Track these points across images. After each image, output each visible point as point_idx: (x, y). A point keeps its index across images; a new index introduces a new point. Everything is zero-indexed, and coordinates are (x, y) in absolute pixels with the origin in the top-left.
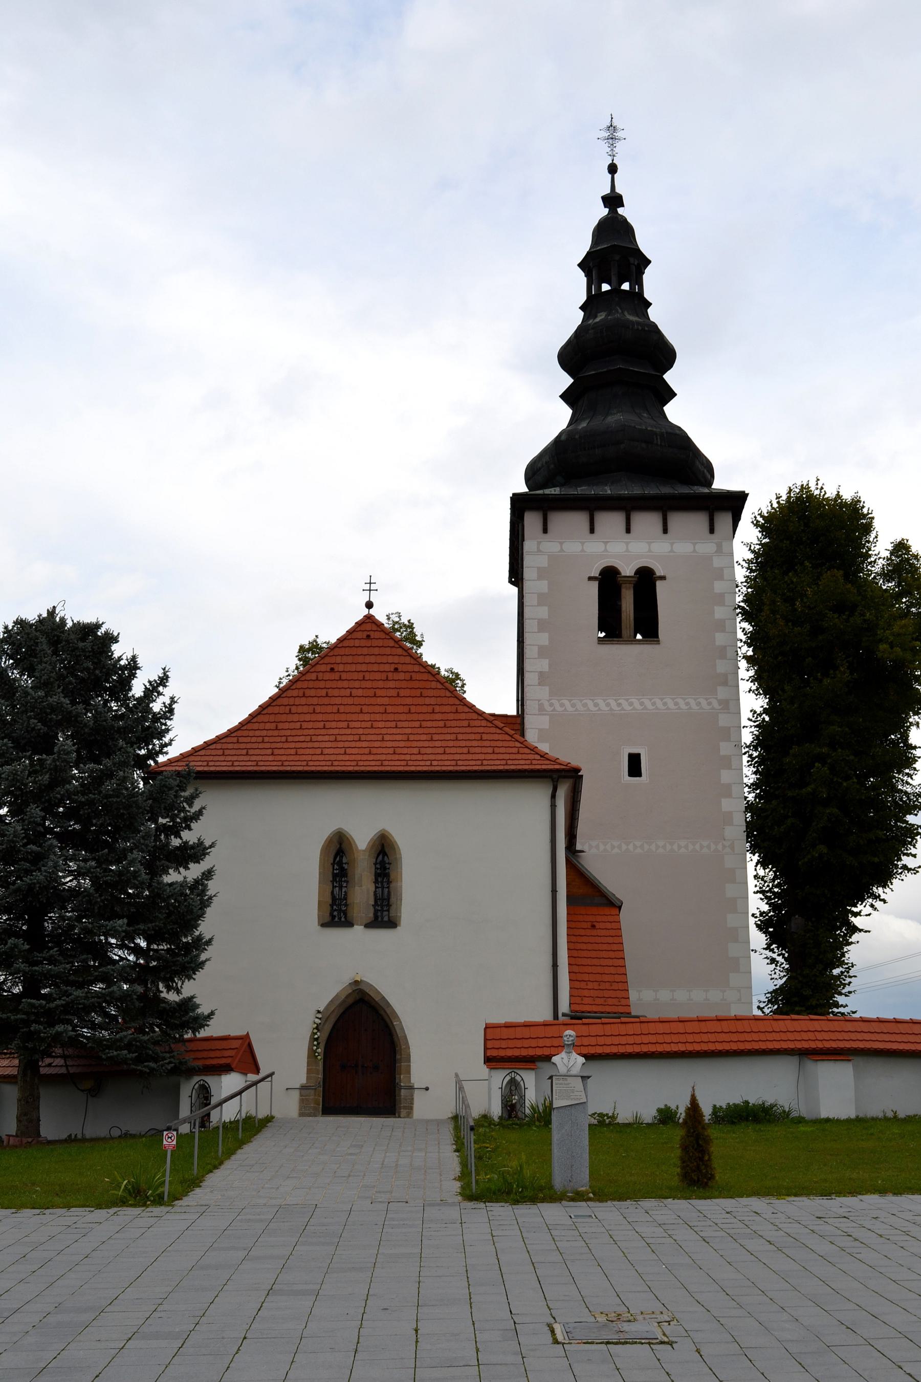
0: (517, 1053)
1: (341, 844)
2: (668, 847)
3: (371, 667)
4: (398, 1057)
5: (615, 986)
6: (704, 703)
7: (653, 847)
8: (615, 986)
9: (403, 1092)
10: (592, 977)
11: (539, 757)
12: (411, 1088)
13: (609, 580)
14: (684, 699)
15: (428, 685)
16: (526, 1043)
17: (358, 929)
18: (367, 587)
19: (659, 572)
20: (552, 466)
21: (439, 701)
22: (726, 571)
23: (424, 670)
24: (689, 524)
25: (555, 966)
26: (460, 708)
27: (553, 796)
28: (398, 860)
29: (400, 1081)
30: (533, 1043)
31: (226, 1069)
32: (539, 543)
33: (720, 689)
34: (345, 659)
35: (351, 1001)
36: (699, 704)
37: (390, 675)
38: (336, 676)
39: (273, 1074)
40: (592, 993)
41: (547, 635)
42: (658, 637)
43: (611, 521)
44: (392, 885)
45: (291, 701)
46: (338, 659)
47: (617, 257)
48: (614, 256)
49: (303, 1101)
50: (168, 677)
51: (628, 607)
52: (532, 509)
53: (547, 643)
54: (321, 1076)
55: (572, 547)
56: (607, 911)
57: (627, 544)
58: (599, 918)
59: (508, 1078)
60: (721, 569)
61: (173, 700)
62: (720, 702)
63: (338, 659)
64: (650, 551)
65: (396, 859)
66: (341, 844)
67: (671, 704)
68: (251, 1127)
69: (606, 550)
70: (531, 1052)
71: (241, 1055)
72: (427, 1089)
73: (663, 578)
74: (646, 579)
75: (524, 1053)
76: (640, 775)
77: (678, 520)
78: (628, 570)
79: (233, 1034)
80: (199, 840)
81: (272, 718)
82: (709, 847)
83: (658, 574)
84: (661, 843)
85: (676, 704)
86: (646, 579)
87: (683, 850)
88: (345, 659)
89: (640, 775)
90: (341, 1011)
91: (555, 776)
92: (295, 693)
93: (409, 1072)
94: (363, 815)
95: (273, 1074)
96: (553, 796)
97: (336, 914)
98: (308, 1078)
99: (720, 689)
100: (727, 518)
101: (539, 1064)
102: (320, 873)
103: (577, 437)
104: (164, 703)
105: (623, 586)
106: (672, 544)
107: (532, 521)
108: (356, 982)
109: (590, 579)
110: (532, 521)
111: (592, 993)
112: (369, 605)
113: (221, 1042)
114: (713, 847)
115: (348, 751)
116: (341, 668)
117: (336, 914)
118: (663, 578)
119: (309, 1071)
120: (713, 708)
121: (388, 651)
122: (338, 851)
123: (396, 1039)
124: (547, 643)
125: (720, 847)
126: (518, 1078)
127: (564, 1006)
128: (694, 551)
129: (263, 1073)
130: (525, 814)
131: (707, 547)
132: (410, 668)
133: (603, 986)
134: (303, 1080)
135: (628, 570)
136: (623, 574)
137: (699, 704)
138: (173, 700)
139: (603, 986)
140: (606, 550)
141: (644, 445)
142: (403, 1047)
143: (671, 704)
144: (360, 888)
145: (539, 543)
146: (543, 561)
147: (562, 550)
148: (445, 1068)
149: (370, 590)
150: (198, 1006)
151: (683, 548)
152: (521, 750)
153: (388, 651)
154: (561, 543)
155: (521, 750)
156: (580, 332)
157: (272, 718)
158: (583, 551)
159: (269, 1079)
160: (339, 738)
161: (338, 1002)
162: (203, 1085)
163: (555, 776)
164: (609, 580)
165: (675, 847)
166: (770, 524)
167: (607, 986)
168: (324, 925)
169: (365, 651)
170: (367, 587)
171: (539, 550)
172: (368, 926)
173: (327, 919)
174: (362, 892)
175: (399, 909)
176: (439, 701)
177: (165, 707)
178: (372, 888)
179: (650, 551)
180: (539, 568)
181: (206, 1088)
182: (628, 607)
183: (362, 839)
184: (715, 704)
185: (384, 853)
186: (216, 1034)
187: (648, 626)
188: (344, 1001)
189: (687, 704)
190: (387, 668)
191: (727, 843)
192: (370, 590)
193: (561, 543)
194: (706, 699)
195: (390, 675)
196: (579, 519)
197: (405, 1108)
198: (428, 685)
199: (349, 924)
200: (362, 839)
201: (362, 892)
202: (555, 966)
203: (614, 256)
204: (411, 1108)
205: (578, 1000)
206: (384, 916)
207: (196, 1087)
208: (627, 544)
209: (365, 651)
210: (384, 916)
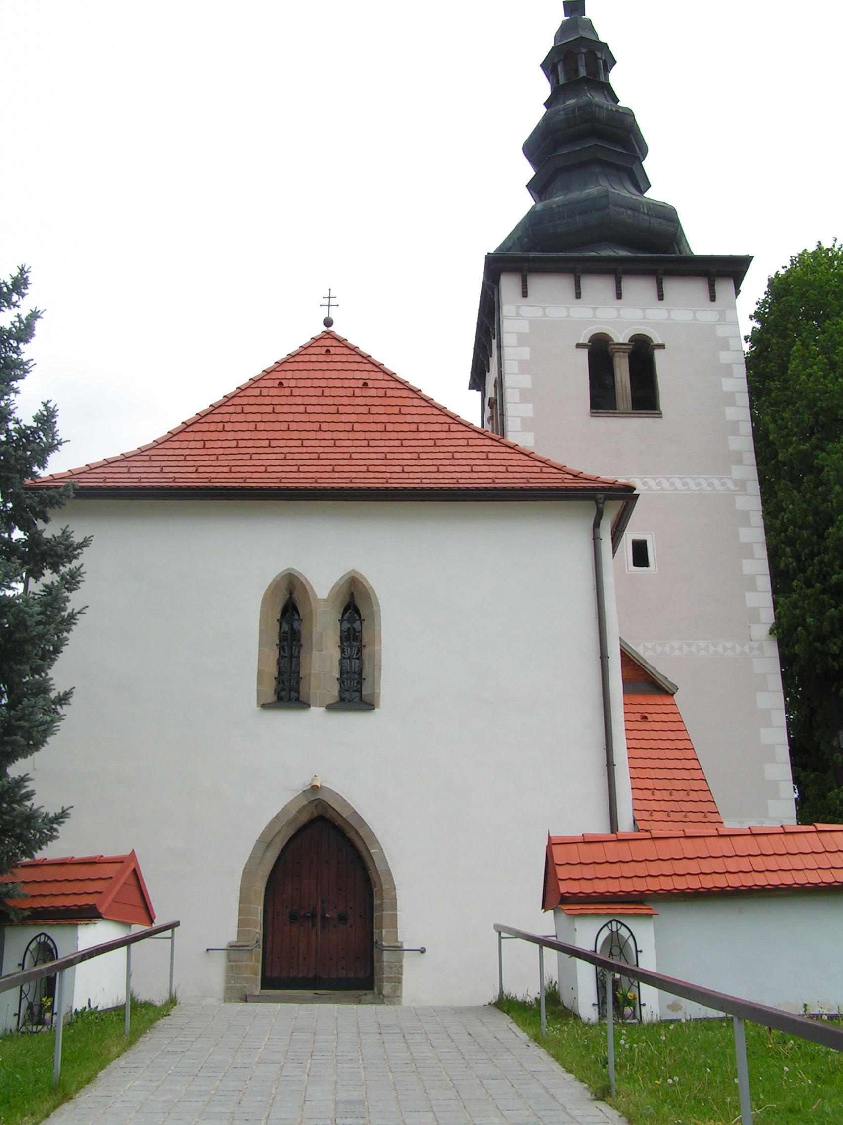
0: (614, 887)
1: (291, 593)
2: (686, 649)
3: (331, 383)
4: (376, 902)
5: (694, 796)
6: (717, 483)
7: (667, 649)
8: (694, 796)
9: (386, 956)
10: (658, 784)
11: (572, 477)
12: (398, 949)
13: (600, 351)
14: (694, 479)
15: (409, 402)
16: (628, 870)
17: (316, 711)
18: (326, 301)
19: (657, 339)
20: (526, 240)
21: (425, 419)
22: (731, 341)
23: (403, 387)
24: (685, 294)
25: (610, 764)
26: (454, 427)
27: (596, 525)
28: (374, 615)
29: (382, 940)
30: (641, 869)
31: (90, 914)
32: (519, 307)
33: (735, 468)
34: (297, 375)
35: (304, 818)
36: (711, 484)
37: (358, 392)
38: (287, 392)
39: (177, 924)
40: (664, 806)
41: (531, 406)
42: (659, 410)
43: (598, 288)
44: (365, 651)
45: (226, 418)
46: (289, 375)
47: (584, 50)
48: (578, 61)
49: (233, 971)
50: (26, 279)
51: (623, 378)
52: (511, 270)
53: (531, 415)
54: (259, 930)
55: (556, 313)
56: (658, 699)
57: (619, 310)
58: (651, 709)
59: (606, 933)
60: (726, 339)
61: (35, 316)
62: (736, 483)
63: (289, 375)
64: (644, 318)
65: (372, 612)
66: (291, 593)
67: (679, 485)
68: (135, 1018)
69: (594, 316)
70: (640, 886)
71: (120, 893)
72: (423, 951)
73: (662, 346)
74: (642, 351)
75: (627, 886)
76: (646, 564)
77: (672, 287)
78: (621, 336)
79: (108, 854)
80: (64, 532)
81: (199, 436)
82: (733, 649)
83: (655, 342)
84: (676, 644)
85: (684, 484)
86: (642, 351)
87: (703, 652)
88: (297, 375)
89: (646, 564)
90: (291, 832)
91: (600, 496)
92: (231, 409)
93: (395, 925)
94: (323, 552)
95: (177, 924)
96: (596, 525)
97: (286, 689)
98: (239, 933)
99: (734, 467)
100: (729, 286)
101: (655, 908)
102: (261, 632)
103: (554, 206)
104: (19, 316)
105: (617, 354)
106: (669, 311)
107: (509, 285)
108: (315, 788)
109: (579, 346)
110: (509, 285)
111: (664, 806)
112: (328, 323)
113: (87, 867)
114: (738, 649)
115: (302, 469)
116: (293, 383)
117: (286, 689)
118: (662, 346)
119: (242, 923)
120: (728, 489)
121: (354, 366)
122: (289, 609)
123: (373, 875)
124: (531, 415)
125: (746, 649)
126: (624, 932)
127: (625, 825)
128: (695, 319)
129: (158, 923)
130: (558, 545)
131: (707, 314)
132: (384, 384)
133: (676, 796)
134: (231, 935)
135: (621, 336)
136: (616, 341)
137: (711, 484)
138: (35, 316)
139: (676, 796)
140: (594, 316)
141: (630, 212)
142: (385, 887)
143: (679, 485)
144: (318, 653)
145: (519, 307)
146: (523, 326)
147: (545, 315)
148: (462, 913)
149: (329, 305)
150: (28, 796)
151: (682, 315)
152: (544, 470)
153: (354, 366)
154: (544, 308)
155: (544, 470)
156: (545, 118)
157: (199, 436)
158: (568, 316)
159: (168, 933)
160: (289, 456)
161: (286, 819)
162: (45, 943)
163: (600, 496)
164: (600, 351)
165: (694, 649)
166: (779, 287)
167: (682, 795)
168: (265, 706)
169: (324, 366)
170: (326, 301)
171: (518, 315)
172: (330, 708)
173: (271, 697)
174: (323, 659)
175: (375, 684)
176: (425, 419)
177: (21, 321)
178: (337, 654)
179: (644, 318)
180: (518, 334)
181: (51, 950)
182: (623, 378)
183: (322, 584)
184: (730, 484)
185: (355, 607)
186: (80, 853)
187: (646, 399)
188: (295, 818)
189: (698, 484)
190: (353, 383)
191: (755, 645)
192: (329, 305)
193: (544, 308)
194: (720, 479)
195: (358, 392)
196: (561, 285)
197: (390, 980)
198: (409, 402)
199: (305, 705)
200: (322, 584)
201: (323, 659)
202: (610, 764)
203: (578, 61)
204: (400, 981)
205: (645, 815)
206: (355, 691)
207: (33, 946)
208: (619, 310)
209: (324, 366)
210: (355, 691)
